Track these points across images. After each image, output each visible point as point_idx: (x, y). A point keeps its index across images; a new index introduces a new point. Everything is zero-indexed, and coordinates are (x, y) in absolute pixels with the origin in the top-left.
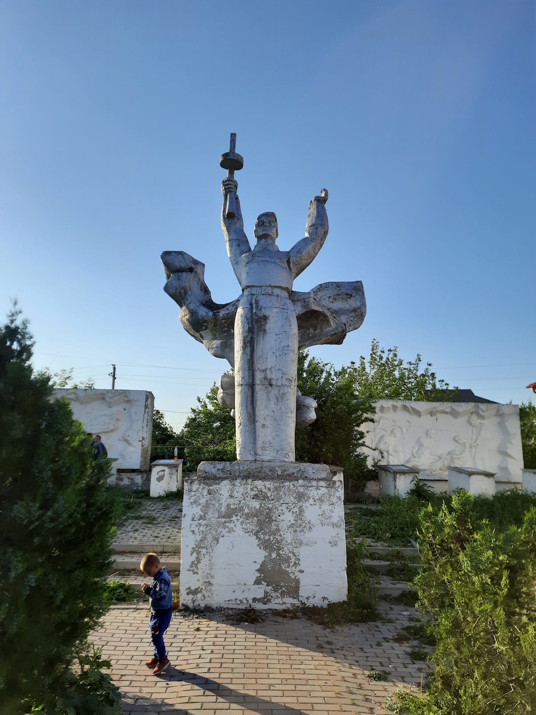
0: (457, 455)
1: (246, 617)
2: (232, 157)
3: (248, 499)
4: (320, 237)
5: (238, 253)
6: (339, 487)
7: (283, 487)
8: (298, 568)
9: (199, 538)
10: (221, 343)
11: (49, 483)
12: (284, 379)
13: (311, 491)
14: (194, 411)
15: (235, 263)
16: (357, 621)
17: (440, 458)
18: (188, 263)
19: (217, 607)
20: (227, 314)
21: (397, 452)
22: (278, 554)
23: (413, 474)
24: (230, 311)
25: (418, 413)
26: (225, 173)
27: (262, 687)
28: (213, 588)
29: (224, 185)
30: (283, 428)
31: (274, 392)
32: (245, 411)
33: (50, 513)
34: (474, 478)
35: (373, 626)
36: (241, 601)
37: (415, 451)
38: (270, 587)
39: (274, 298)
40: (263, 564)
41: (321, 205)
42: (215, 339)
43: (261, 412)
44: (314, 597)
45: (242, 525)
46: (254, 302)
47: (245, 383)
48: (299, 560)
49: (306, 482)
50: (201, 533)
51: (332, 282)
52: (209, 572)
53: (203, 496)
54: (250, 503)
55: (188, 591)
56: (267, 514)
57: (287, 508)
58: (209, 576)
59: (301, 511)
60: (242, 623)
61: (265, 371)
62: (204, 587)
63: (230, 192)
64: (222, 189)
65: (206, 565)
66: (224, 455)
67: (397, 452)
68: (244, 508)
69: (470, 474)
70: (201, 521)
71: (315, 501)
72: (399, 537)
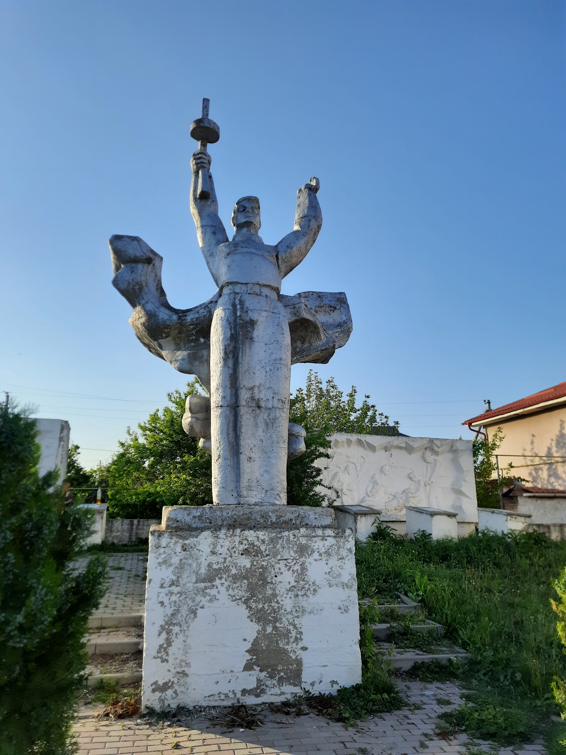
0: (412, 494)
1: (236, 719)
2: (206, 125)
3: (236, 555)
4: (314, 231)
5: (214, 242)
6: (349, 536)
7: (281, 538)
8: (301, 645)
9: (169, 611)
10: (189, 354)
11: (9, 554)
12: (275, 401)
13: (315, 542)
14: (122, 445)
15: (209, 254)
16: (380, 712)
17: (395, 496)
18: (145, 252)
19: (194, 707)
20: (197, 318)
21: (351, 491)
22: (275, 628)
23: (374, 515)
24: (202, 315)
25: (372, 448)
26: (197, 146)
27: (141, 743)
28: (189, 680)
29: (195, 159)
30: (274, 461)
31: (263, 416)
32: (226, 440)
33: (20, 618)
34: (436, 518)
35: (401, 716)
36: (227, 696)
37: (369, 490)
38: (264, 673)
39: (264, 299)
40: (256, 642)
41: (313, 194)
42: (179, 349)
43: (249, 441)
44: (321, 681)
45: (228, 590)
46: (237, 302)
47: (226, 404)
48: (301, 633)
49: (309, 531)
50: (173, 604)
51: (313, 292)
52: (184, 658)
53: (175, 553)
54: (238, 561)
55: (154, 687)
56: (261, 574)
57: (286, 565)
58: (184, 664)
59: (304, 569)
60: (235, 729)
61: (252, 389)
62: (175, 680)
63: (203, 167)
64: (192, 164)
65: (179, 649)
66: (157, 498)
67: (351, 491)
68: (231, 568)
69: (433, 514)
70: (173, 587)
71: (320, 555)
72: (385, 591)
